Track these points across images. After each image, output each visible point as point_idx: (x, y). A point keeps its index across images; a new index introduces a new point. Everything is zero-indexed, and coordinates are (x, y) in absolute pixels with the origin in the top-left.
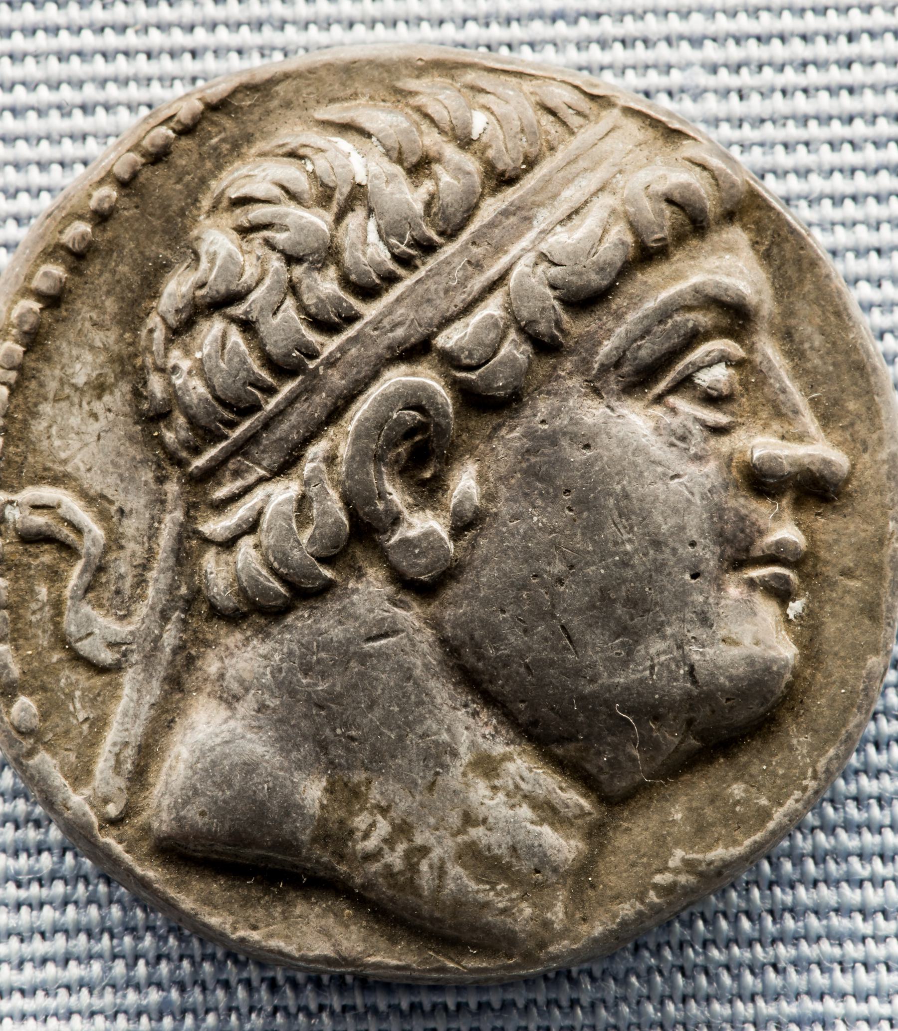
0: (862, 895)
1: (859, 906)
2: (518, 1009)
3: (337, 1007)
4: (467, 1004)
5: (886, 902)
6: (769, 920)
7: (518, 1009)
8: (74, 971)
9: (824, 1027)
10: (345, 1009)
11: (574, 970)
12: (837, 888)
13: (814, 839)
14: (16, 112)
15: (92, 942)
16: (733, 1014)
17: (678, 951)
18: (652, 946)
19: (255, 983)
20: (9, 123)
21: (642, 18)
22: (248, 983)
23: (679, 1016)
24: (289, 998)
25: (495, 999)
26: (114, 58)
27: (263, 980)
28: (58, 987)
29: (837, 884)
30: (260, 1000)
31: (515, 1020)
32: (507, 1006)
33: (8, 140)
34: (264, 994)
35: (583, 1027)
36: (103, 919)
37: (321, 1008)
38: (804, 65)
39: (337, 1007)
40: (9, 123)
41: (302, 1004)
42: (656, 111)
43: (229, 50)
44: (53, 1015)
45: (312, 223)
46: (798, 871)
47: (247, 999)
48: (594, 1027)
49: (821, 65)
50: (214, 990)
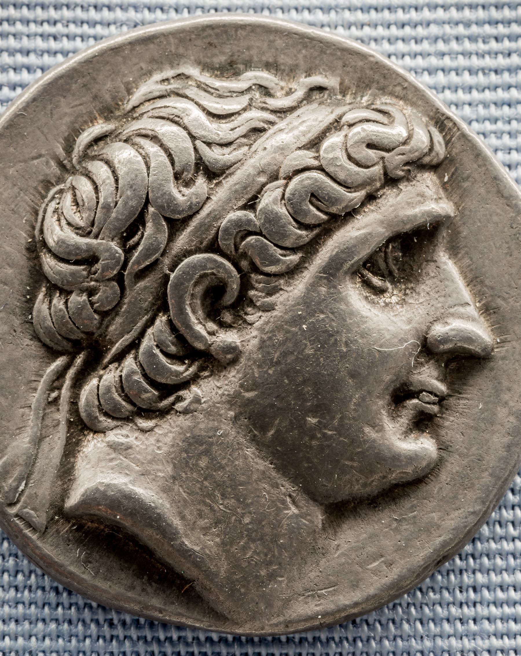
0: (502, 577)
2: (308, 642)
3: (135, 637)
5: (515, 580)
7: (308, 642)
10: (139, 638)
11: (358, 620)
12: (488, 574)
14: (12, 53)
16: (434, 647)
20: (6, 59)
21: (483, 56)
22: (97, 622)
23: (419, 647)
24: (106, 630)
25: (310, 636)
26: (21, 8)
27: (105, 620)
28: (417, 652)
29: (488, 571)
31: (319, 649)
33: (3, 69)
34: (106, 628)
35: (362, 653)
38: (415, 55)
39: (135, 637)
40: (6, 59)
43: (464, 104)
47: (83, 630)
48: (354, 654)
49: (424, 55)
50: (130, 628)
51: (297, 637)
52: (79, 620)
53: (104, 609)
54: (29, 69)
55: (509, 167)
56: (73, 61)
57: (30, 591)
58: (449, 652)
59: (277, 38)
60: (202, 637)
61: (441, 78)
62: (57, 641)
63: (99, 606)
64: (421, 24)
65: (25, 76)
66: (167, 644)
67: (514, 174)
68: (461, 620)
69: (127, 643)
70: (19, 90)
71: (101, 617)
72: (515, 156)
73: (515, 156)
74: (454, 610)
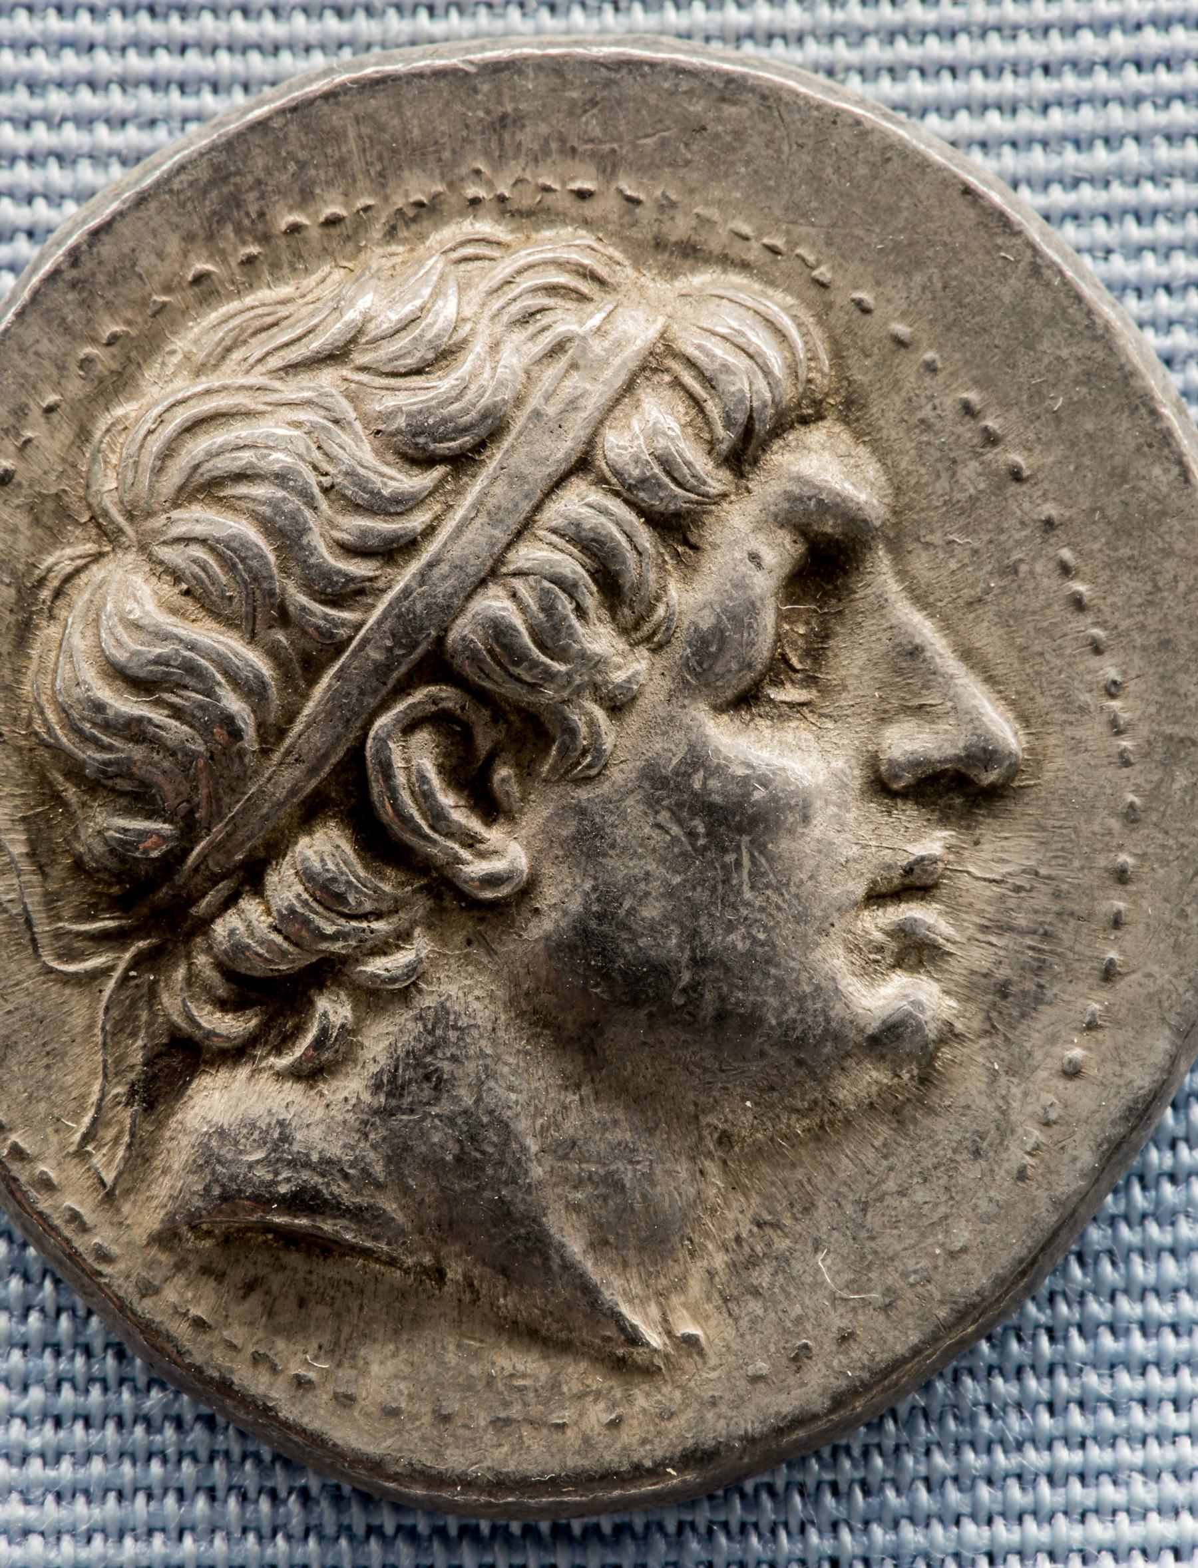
1: (1079, 1469)
4: (568, 1526)
6: (1044, 1341)
8: (65, 1470)
9: (1022, 1560)
13: (1144, 1231)
15: (92, 1431)
17: (891, 1459)
18: (856, 1451)
19: (283, 1494)
22: (273, 1495)
24: (325, 1512)
30: (288, 1515)
32: (621, 1530)
35: (759, 1563)
36: (138, 1407)
37: (371, 1530)
39: (390, 1529)
41: (346, 1522)
42: (1076, 271)
44: (68, 1532)
45: (612, 539)
46: (1184, 1124)
51: (577, 1526)
52: (230, 1488)
53: (287, 1464)
54: (98, 158)
55: (1168, 362)
56: (198, 138)
57: (88, 1425)
58: (927, 1556)
59: (1165, 489)
60: (423, 1527)
61: (1059, 197)
62: (212, 1541)
63: (276, 1458)
64: (1060, 104)
65: (86, 173)
66: (436, 1545)
67: (1176, 380)
68: (1019, 1477)
69: (374, 1545)
70: (70, 207)
71: (280, 1479)
72: (1181, 338)
73: (1181, 338)
74: (1065, 1456)
